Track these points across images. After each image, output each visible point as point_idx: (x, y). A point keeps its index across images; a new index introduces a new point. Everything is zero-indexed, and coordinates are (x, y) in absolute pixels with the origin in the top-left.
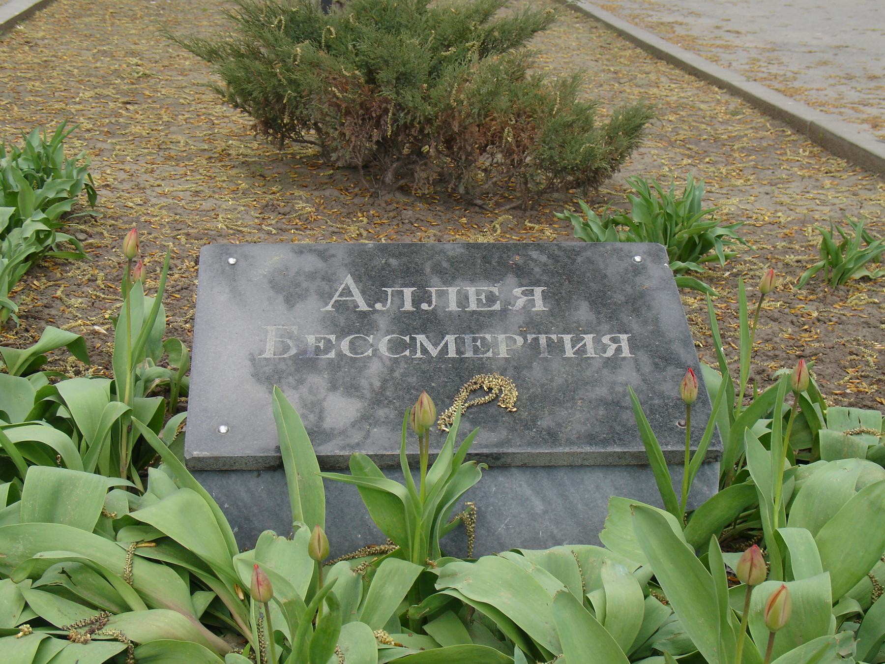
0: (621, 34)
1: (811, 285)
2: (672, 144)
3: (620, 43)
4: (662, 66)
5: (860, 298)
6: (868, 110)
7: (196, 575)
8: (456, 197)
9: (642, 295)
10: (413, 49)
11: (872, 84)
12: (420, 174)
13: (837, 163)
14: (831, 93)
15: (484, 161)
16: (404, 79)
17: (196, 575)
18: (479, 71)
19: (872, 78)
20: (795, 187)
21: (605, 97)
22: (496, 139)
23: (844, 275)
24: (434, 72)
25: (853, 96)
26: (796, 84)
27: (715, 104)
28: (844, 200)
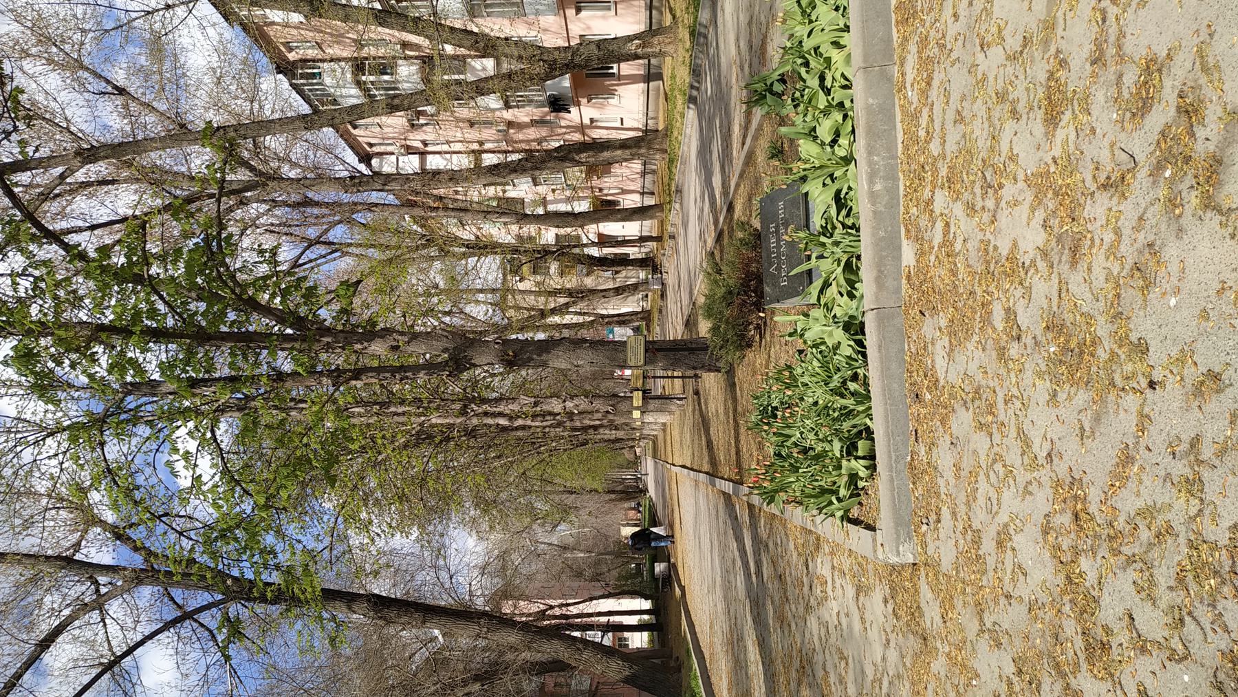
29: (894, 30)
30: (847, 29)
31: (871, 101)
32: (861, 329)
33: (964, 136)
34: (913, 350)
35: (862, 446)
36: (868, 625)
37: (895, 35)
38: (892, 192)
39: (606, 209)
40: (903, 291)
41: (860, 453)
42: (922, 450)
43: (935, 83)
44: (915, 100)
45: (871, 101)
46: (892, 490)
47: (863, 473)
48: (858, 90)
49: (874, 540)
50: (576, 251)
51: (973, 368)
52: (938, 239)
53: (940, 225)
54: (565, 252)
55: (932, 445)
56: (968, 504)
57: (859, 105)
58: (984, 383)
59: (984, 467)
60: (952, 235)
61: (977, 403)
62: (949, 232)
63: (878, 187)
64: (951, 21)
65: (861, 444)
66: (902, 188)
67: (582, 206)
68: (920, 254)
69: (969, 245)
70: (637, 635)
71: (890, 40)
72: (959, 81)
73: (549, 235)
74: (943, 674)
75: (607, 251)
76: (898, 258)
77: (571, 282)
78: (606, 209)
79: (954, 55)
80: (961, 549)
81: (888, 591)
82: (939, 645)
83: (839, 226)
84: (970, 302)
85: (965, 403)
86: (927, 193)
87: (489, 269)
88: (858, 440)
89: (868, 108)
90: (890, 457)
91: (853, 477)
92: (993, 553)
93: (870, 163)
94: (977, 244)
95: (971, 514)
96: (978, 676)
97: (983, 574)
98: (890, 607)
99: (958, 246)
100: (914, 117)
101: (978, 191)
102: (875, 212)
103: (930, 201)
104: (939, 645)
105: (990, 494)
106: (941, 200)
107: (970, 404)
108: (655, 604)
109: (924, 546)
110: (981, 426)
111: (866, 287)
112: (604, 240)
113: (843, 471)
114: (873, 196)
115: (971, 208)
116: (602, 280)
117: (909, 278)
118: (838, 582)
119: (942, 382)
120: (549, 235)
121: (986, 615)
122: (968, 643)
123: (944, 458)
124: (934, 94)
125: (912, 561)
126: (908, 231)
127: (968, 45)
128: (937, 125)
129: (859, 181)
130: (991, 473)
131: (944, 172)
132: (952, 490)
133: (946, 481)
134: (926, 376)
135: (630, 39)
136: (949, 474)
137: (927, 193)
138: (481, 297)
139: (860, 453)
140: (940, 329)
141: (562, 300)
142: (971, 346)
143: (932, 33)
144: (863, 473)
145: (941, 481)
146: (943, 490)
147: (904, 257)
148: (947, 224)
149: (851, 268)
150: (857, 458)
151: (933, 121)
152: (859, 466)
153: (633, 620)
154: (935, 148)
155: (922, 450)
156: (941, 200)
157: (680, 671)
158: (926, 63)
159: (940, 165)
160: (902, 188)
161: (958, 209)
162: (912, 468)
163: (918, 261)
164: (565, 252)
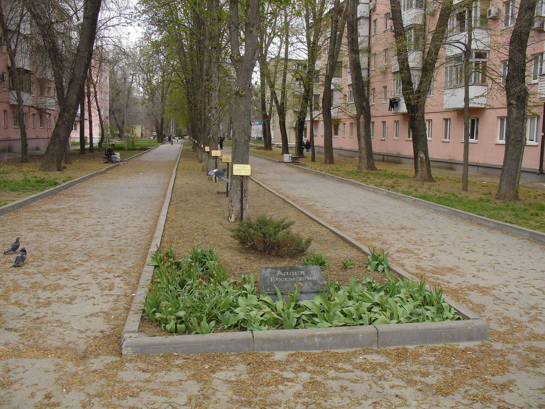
0: (302, 212)
1: (341, 269)
2: (316, 242)
3: (302, 214)
4: (312, 221)
5: (349, 271)
6: (356, 230)
7: (269, 305)
8: (280, 256)
9: (259, 221)
10: (272, 230)
11: (357, 223)
12: (273, 252)
13: (348, 245)
14: (348, 226)
15: (284, 249)
16: (270, 236)
17: (269, 305)
18: (282, 234)
19: (358, 221)
20: (340, 250)
21: (305, 236)
22: (286, 245)
23: (346, 268)
24: (275, 233)
25: (353, 226)
26: (341, 224)
27: (323, 231)
28: (348, 253)
29: (394, 347)
30: (399, 322)
31: (361, 336)
32: (243, 329)
33: (334, 392)
34: (231, 357)
35: (181, 327)
36: (89, 319)
37: (392, 348)
38: (314, 347)
39: (332, 126)
40: (261, 352)
41: (178, 326)
42: (179, 362)
43: (364, 374)
44: (358, 361)
45: (361, 336)
46: (159, 345)
47: (168, 327)
48: (368, 329)
49: (133, 332)
50: (308, 109)
51: (219, 395)
52: (286, 374)
53: (292, 375)
54: (307, 96)
55: (181, 368)
56: (152, 390)
57: (359, 329)
58: (212, 400)
59: (171, 400)
60: (286, 383)
61: (202, 397)
62: (289, 381)
63: (316, 340)
64: (391, 384)
65: (183, 326)
66: (315, 351)
67: (334, 113)
68: (279, 364)
69: (280, 394)
70: (78, 136)
71: (390, 345)
72: (361, 389)
73: (319, 90)
74: (67, 369)
75: (308, 125)
76: (279, 349)
77: (290, 100)
78: (332, 126)
79: (374, 386)
80: (130, 384)
81: (108, 333)
82: (82, 367)
83: (299, 316)
84: (252, 395)
85: (202, 390)
86: (310, 368)
87: (300, 53)
88: (185, 327)
89: (356, 335)
90: (176, 344)
91: (166, 321)
92: (128, 405)
93: (329, 336)
94: (280, 399)
95: (147, 391)
96: (68, 392)
97: (118, 398)
98: (99, 334)
99: (281, 387)
100: (348, 360)
101: (306, 400)
102: (303, 338)
103: (305, 370)
104: (82, 367)
105: (156, 403)
106: (305, 376)
107: (201, 392)
108: (96, 149)
109: (131, 361)
110: (190, 399)
111: (266, 332)
112: (314, 123)
113: (169, 316)
114: (312, 337)
115: (298, 395)
116: (291, 119)
117: (268, 356)
118: (110, 299)
119: (213, 375)
120: (319, 90)
121: (97, 399)
122: (83, 387)
123: (175, 376)
124: (358, 373)
125: (123, 353)
126: (292, 355)
127: (377, 394)
128: (343, 375)
129: (322, 329)
130: (167, 405)
131: (319, 378)
132: (159, 380)
133: (164, 376)
134: (217, 365)
135: (426, 154)
136: (167, 378)
137: (310, 368)
138: (283, 50)
139: (178, 326)
140: (240, 375)
141: (279, 99)
142: (230, 393)
143: (388, 372)
144: (168, 327)
145: (163, 373)
146: (159, 374)
147: (280, 353)
148: (292, 381)
149: (277, 324)
150: (176, 324)
151: (345, 372)
152: (171, 325)
153: (87, 133)
154: (332, 373)
155: (179, 362)
156: (305, 376)
157: (59, 170)
158: (373, 368)
159: (323, 376)
160: (315, 351)
161: (299, 387)
162: (171, 355)
163: (276, 362)
164: (307, 96)
